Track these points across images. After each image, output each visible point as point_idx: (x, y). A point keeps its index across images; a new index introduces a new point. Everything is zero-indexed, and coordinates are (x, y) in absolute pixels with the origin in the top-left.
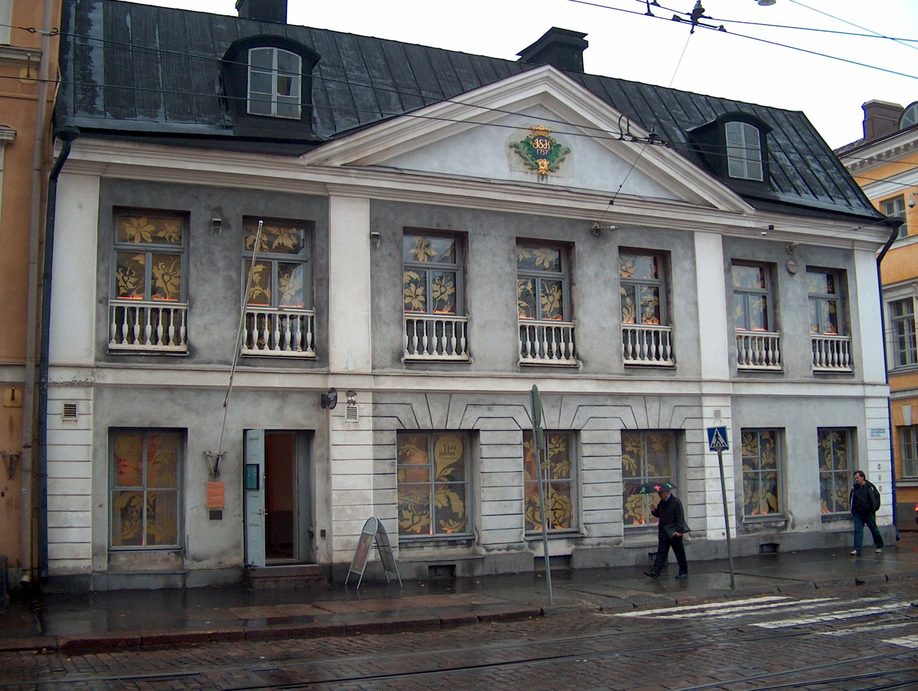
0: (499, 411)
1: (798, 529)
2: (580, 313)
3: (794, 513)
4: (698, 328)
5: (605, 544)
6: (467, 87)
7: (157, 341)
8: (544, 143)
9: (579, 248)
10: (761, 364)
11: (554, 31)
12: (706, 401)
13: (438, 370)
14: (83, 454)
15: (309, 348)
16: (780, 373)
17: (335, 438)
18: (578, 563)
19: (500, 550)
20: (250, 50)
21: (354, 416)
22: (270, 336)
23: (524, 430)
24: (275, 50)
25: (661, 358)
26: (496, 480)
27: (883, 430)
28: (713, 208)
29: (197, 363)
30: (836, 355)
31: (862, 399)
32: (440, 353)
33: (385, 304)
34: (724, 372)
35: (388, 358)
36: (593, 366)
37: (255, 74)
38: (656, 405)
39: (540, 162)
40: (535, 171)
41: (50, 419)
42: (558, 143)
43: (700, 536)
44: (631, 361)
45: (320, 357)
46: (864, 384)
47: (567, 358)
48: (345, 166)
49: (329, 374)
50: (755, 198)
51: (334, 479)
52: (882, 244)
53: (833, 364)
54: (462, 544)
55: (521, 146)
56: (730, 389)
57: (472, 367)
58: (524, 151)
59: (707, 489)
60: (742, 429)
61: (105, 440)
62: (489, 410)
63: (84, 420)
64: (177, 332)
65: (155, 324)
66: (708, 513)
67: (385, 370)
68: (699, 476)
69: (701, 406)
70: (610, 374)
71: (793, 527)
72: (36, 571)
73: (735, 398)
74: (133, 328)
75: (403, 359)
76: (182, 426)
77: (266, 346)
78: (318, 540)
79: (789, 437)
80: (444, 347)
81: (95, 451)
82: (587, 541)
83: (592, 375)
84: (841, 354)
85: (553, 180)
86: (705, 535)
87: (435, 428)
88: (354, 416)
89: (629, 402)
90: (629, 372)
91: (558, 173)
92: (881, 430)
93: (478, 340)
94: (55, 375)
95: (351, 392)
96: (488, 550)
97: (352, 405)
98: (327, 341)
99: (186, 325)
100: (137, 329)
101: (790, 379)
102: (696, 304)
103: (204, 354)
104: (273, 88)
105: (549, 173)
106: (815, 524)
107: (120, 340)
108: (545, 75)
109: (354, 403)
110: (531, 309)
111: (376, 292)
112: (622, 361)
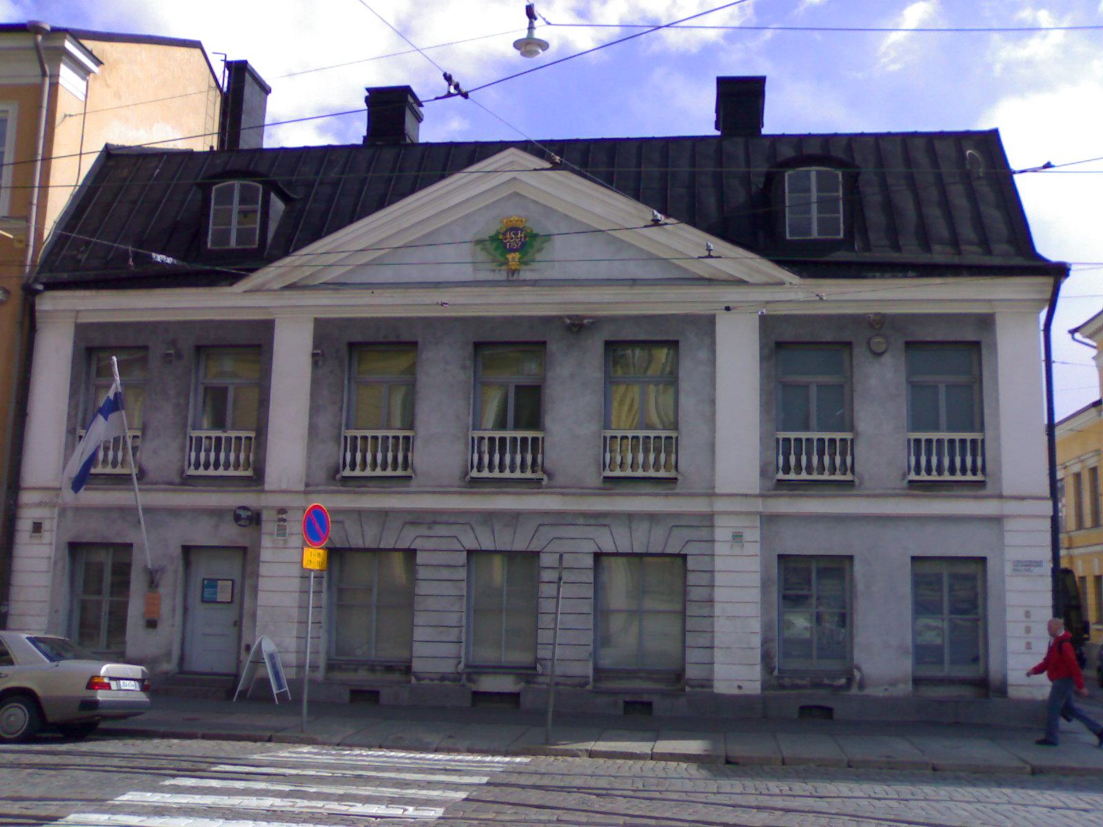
0: (440, 530)
1: (869, 691)
2: (548, 421)
3: (865, 667)
4: (713, 430)
5: (566, 685)
6: (920, 143)
7: (824, 470)
9: (552, 347)
10: (844, 474)
12: (719, 521)
13: (374, 487)
14: (43, 565)
16: (850, 484)
17: (265, 555)
18: (526, 701)
19: (432, 680)
20: (841, 236)
21: (284, 535)
23: (467, 550)
25: (969, 472)
26: (432, 603)
27: (1038, 564)
29: (147, 484)
31: (998, 520)
32: (809, 473)
33: (325, 421)
34: (752, 482)
35: (321, 475)
36: (560, 480)
38: (645, 526)
39: (510, 256)
40: (504, 267)
43: (703, 686)
44: (608, 473)
45: (257, 479)
49: (263, 491)
50: (805, 263)
51: (260, 595)
52: (1045, 300)
54: (400, 670)
56: (759, 506)
57: (414, 482)
59: (716, 629)
61: (65, 552)
62: (430, 528)
63: (47, 536)
64: (844, 462)
65: (821, 454)
66: (716, 660)
67: (320, 488)
68: (706, 612)
69: (712, 526)
70: (582, 488)
71: (862, 686)
73: (769, 520)
74: (386, 457)
75: (338, 476)
76: (129, 542)
77: (119, 465)
79: (858, 568)
81: (55, 563)
82: (541, 679)
83: (559, 490)
85: (526, 275)
86: (712, 687)
87: (367, 547)
88: (284, 535)
89: (607, 521)
90: (608, 485)
91: (534, 265)
93: (420, 457)
94: (26, 497)
95: (282, 511)
96: (419, 679)
97: (282, 523)
98: (265, 461)
99: (852, 454)
100: (958, 460)
101: (866, 492)
102: (713, 402)
103: (152, 475)
104: (230, 221)
105: (523, 267)
106: (901, 686)
107: (480, 469)
108: (510, 159)
109: (284, 520)
111: (314, 410)
112: (600, 474)
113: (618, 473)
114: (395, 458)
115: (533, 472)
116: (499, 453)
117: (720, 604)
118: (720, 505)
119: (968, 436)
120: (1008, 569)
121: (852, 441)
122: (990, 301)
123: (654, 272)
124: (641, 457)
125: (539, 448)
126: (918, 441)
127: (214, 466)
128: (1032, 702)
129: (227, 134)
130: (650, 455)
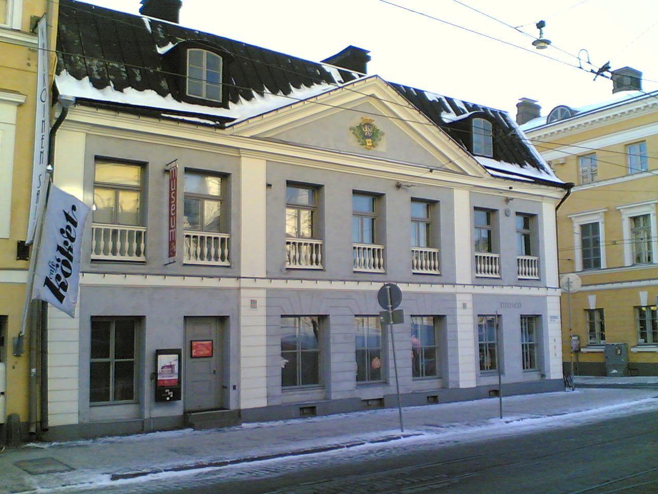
8: (370, 128)
11: (350, 47)
15: (226, 259)
22: (121, 245)
24: (205, 51)
28: (464, 173)
30: (428, 262)
37: (192, 67)
39: (367, 140)
41: (242, 309)
42: (378, 128)
46: (547, 288)
47: (317, 265)
48: (252, 137)
53: (485, 272)
55: (356, 130)
58: (358, 133)
60: (92, 317)
72: (39, 424)
78: (232, 393)
80: (94, 249)
84: (534, 268)
92: (555, 317)
100: (206, 250)
110: (477, 250)
113: (102, 257)
114: (209, 252)
115: (312, 264)
116: (104, 241)
117: (277, 344)
118: (244, 283)
119: (220, 236)
120: (549, 319)
121: (145, 233)
122: (238, 148)
123: (459, 171)
124: (102, 243)
125: (225, 245)
126: (98, 230)
127: (221, 258)
128: (179, 416)
129: (229, 52)
130: (109, 243)
